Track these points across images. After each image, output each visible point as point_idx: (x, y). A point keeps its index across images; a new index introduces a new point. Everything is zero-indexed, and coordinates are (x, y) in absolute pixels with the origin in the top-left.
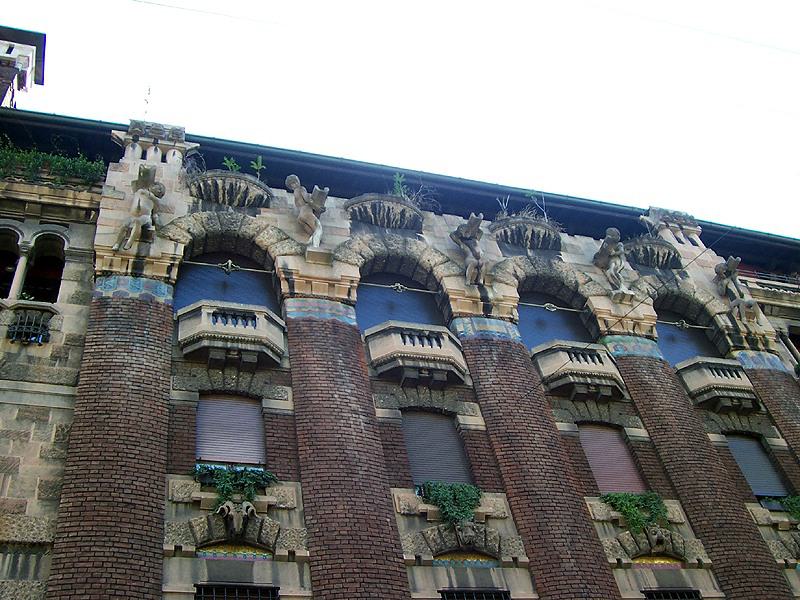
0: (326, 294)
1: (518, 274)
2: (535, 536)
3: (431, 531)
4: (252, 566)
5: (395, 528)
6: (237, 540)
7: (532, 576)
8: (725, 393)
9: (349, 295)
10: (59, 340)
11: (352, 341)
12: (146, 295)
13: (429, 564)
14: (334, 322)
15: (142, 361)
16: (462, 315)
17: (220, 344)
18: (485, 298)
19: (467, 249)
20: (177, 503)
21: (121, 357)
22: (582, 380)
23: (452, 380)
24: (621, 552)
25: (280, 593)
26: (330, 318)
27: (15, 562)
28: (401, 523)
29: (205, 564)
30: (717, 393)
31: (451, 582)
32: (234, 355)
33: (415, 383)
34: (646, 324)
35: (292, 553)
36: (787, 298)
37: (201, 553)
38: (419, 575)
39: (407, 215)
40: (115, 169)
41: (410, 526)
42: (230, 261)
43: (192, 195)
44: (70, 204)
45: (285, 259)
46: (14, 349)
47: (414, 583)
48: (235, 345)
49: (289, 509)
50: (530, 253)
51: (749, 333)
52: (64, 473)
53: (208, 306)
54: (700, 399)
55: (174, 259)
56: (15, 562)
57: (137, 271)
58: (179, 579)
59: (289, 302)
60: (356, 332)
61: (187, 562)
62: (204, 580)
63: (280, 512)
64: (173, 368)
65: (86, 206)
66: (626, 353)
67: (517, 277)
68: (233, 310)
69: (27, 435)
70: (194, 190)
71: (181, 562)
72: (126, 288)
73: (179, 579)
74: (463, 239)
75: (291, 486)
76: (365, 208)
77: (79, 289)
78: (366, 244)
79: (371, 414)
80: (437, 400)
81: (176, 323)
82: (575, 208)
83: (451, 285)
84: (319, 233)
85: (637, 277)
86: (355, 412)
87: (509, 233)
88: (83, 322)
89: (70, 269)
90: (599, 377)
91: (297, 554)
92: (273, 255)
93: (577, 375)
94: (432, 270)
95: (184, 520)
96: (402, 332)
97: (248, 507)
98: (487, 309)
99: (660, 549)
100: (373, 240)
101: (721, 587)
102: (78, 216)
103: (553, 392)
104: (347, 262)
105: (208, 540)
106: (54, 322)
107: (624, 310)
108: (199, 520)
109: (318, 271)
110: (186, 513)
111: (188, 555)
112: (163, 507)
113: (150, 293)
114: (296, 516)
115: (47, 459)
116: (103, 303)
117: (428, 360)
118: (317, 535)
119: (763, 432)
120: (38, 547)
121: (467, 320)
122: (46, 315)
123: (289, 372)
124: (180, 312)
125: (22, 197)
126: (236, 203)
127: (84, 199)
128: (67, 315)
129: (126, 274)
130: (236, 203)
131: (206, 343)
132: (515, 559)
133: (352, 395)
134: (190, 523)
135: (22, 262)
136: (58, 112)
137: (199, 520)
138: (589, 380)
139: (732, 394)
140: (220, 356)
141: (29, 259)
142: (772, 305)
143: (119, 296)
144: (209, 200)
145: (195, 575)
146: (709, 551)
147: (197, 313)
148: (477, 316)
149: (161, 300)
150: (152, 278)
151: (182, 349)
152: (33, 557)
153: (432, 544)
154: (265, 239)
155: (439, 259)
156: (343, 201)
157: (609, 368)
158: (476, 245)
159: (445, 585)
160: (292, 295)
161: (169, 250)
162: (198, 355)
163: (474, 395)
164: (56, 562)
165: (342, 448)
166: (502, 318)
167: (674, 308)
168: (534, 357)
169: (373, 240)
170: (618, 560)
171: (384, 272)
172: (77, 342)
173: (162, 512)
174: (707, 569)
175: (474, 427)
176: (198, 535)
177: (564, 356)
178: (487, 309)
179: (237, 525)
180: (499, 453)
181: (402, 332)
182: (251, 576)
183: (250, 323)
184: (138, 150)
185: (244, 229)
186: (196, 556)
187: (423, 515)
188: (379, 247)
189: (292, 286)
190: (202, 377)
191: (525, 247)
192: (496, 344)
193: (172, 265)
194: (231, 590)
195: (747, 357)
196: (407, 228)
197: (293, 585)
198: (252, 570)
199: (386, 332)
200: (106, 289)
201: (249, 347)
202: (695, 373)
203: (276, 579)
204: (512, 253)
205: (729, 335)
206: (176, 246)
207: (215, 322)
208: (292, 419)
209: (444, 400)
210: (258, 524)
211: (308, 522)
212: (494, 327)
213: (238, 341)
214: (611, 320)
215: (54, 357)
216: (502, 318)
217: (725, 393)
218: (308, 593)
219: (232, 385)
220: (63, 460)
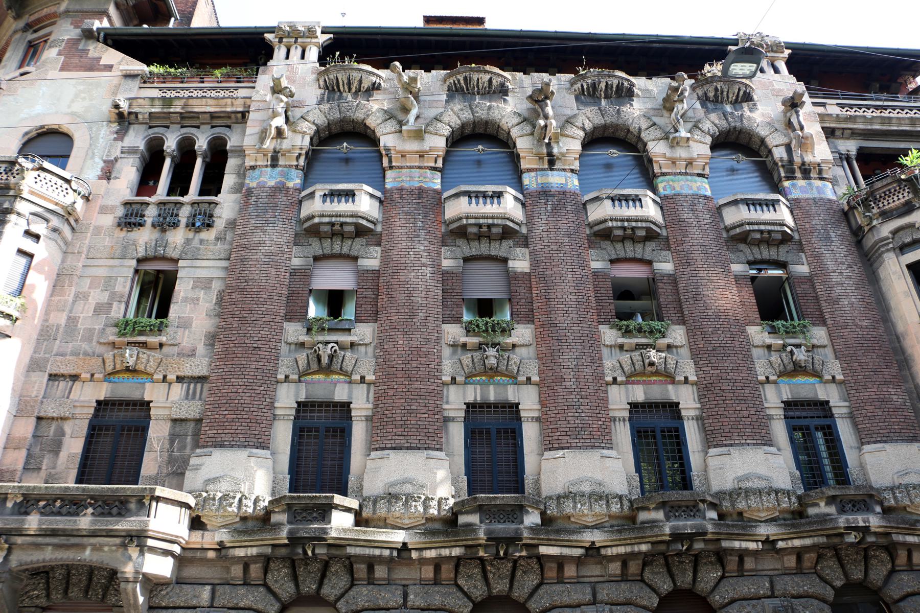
0: (417, 164)
1: (586, 126)
2: (548, 359)
3: (775, 357)
5: (440, 357)
6: (327, 370)
7: (540, 391)
8: (756, 227)
9: (436, 162)
10: (220, 224)
11: (437, 201)
12: (280, 182)
13: (775, 382)
14: (420, 189)
15: (274, 237)
16: (529, 170)
17: (326, 220)
18: (550, 154)
19: (540, 110)
20: (290, 344)
21: (258, 237)
22: (619, 224)
23: (507, 233)
24: (619, 371)
25: (520, 407)
26: (417, 185)
27: (188, 389)
28: (447, 351)
30: (610, 224)
31: (475, 397)
32: (337, 227)
33: (758, 243)
34: (701, 162)
35: (363, 378)
36: (862, 120)
37: (302, 379)
38: (614, 391)
39: (494, 82)
40: (264, 72)
41: (454, 353)
42: (345, 144)
43: (320, 88)
44: (229, 110)
45: (387, 140)
46: (191, 235)
47: (447, 397)
48: (338, 219)
49: (366, 345)
50: (603, 102)
51: (803, 164)
52: (218, 327)
53: (321, 189)
54: (732, 233)
55: (301, 149)
56: (188, 389)
57: (274, 163)
59: (389, 173)
60: (438, 193)
61: (292, 386)
62: (302, 398)
64: (297, 240)
65: (240, 109)
66: (673, 192)
67: (583, 129)
68: (338, 190)
69: (198, 300)
70: (322, 83)
72: (269, 178)
74: (537, 101)
76: (459, 81)
77: (237, 180)
78: (456, 115)
79: (437, 265)
80: (496, 249)
81: (300, 202)
82: (661, 45)
83: (523, 145)
84: (414, 112)
85: (703, 115)
86: (424, 265)
87: (585, 87)
88: (237, 208)
89: (232, 163)
90: (637, 221)
92: (378, 134)
93: (616, 220)
94: (509, 133)
96: (468, 194)
98: (552, 163)
99: (653, 369)
100: (462, 110)
101: (699, 399)
102: (237, 118)
103: (597, 234)
104: (436, 134)
106: (217, 212)
107: (681, 153)
109: (413, 146)
110: (296, 350)
111: (294, 382)
113: (283, 180)
114: (370, 349)
115: (210, 316)
116: (249, 192)
117: (487, 218)
118: (383, 365)
119: (789, 259)
120: (202, 379)
121: (533, 174)
122: (212, 206)
123: (667, 238)
124: (303, 194)
125: (196, 110)
126: (354, 90)
128: (226, 203)
129: (267, 166)
130: (354, 90)
131: (317, 220)
132: (833, 377)
133: (424, 251)
135: (168, 163)
136: (807, 42)
137: (302, 357)
138: (626, 224)
139: (762, 227)
140: (326, 228)
141: (173, 158)
142: (844, 129)
143: (261, 186)
144: (334, 90)
145: (297, 395)
146: (698, 368)
147: (312, 195)
148: (543, 170)
149: (290, 184)
150: (286, 166)
151: (448, 225)
152: (192, 385)
153: (466, 368)
154: (372, 122)
155: (516, 120)
156: (438, 74)
157: (784, 214)
158: (547, 105)
159: (470, 399)
160: (391, 168)
161: (299, 141)
162: (312, 231)
163: (525, 242)
164: (211, 389)
165: (409, 295)
166: (564, 170)
167: (734, 142)
168: (721, 206)
169: (462, 110)
170: (767, 378)
171: (477, 137)
172: (232, 225)
174: (692, 384)
175: (519, 270)
177: (608, 203)
178: (552, 163)
179: (325, 360)
180: (535, 292)
181: (468, 194)
182: (334, 394)
183: (350, 199)
184: (283, 50)
185: (357, 114)
186: (300, 381)
187: (464, 346)
188: (467, 116)
189: (390, 161)
190: (316, 247)
191: (599, 98)
192: (553, 196)
193: (300, 154)
194: (321, 404)
195: (798, 188)
196: (494, 92)
199: (457, 195)
200: (251, 182)
201: (348, 220)
202: (733, 208)
203: (350, 396)
204: (586, 104)
205: (783, 166)
206: (303, 138)
207: (324, 201)
208: (376, 274)
209: (496, 249)
212: (556, 179)
213: (340, 216)
214: (662, 162)
215: (217, 239)
216: (564, 170)
217: (756, 227)
218: (371, 406)
219: (630, 254)
220: (218, 315)
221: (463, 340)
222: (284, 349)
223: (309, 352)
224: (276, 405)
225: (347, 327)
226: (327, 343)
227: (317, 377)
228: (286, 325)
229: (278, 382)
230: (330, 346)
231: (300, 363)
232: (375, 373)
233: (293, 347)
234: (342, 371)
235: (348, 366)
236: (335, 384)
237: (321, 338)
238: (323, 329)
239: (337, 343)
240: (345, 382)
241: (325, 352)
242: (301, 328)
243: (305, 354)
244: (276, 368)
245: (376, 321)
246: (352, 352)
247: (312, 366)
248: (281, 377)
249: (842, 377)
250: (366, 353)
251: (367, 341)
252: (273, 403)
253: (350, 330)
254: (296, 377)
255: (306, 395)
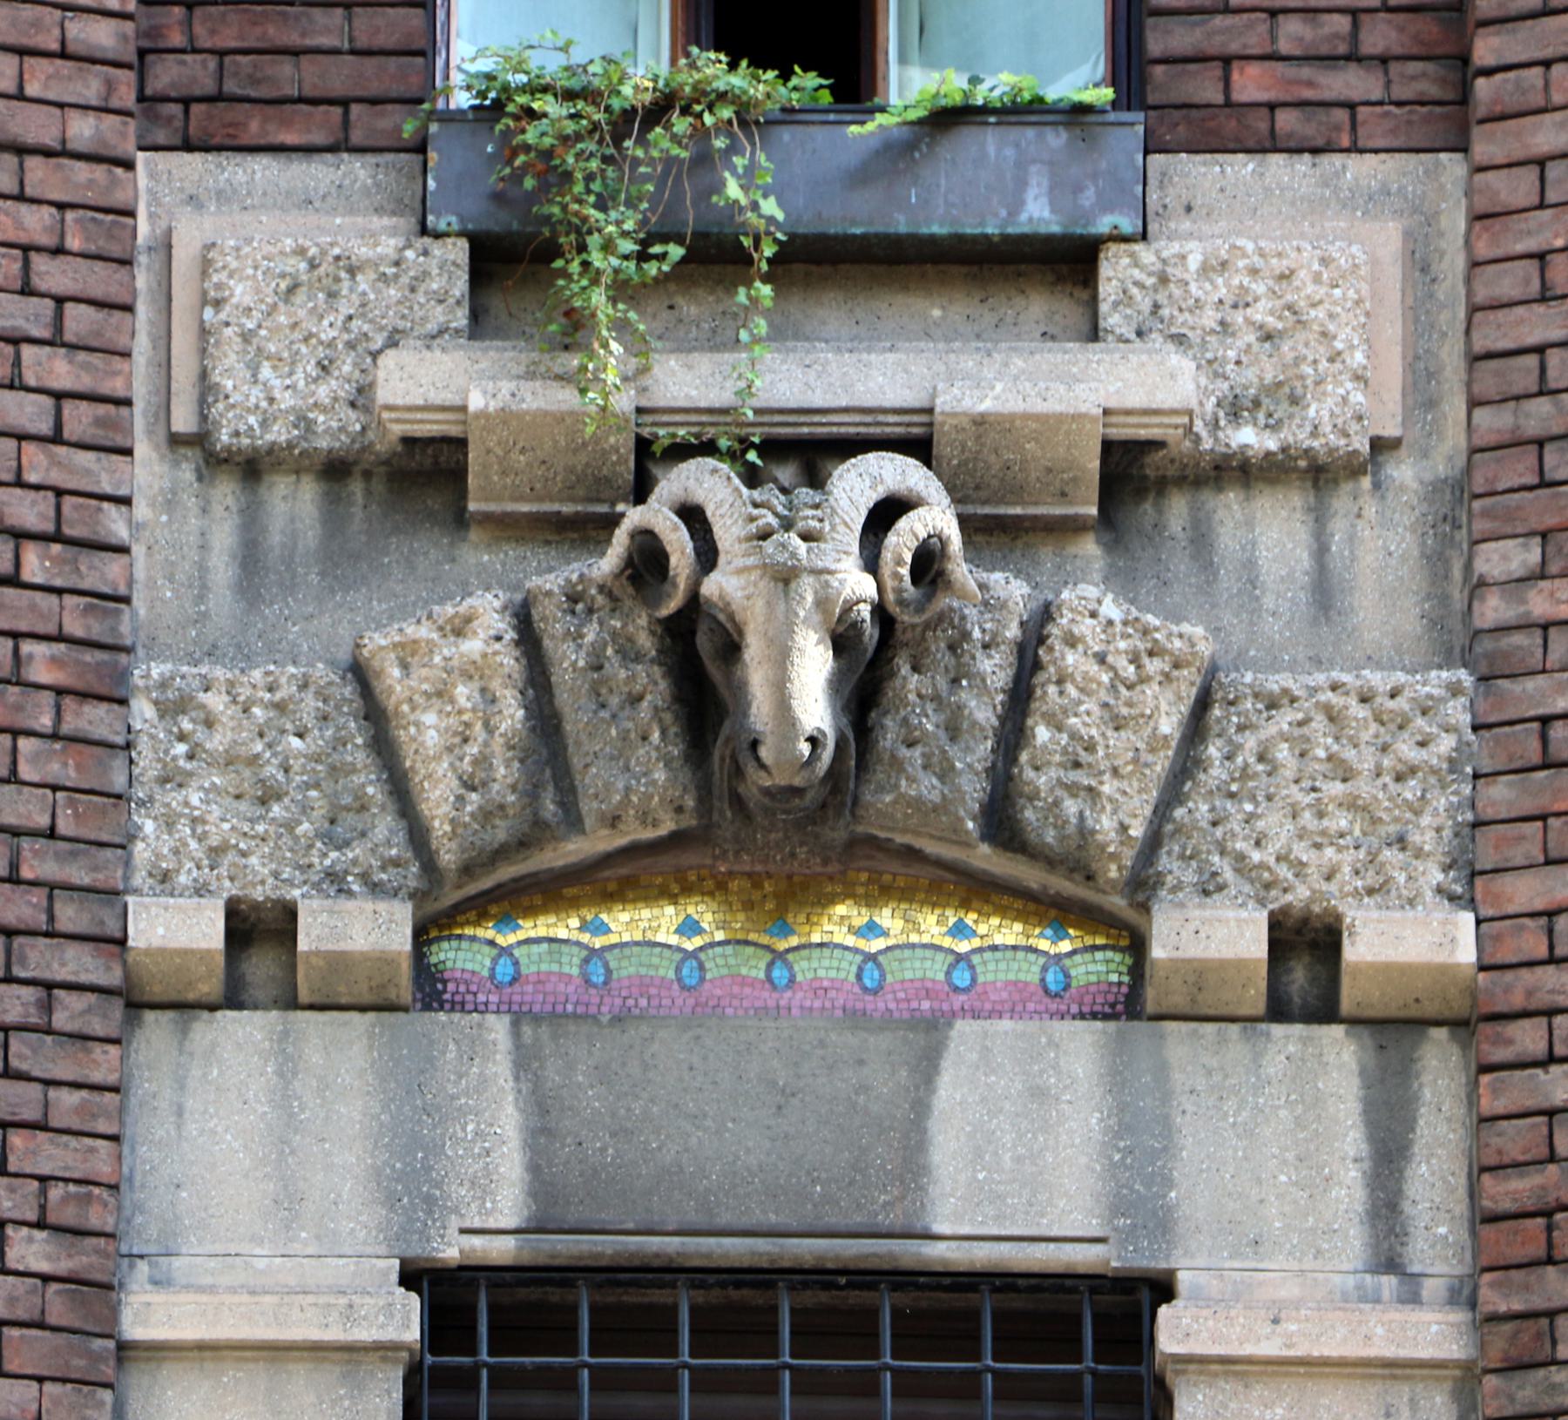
4: (927, 1066)
6: (773, 835)
20: (251, 468)
25: (1176, 1331)
29: (501, 1068)
35: (1306, 948)
37: (464, 956)
49: (1318, 475)
58: (278, 1204)
61: (341, 1050)
62: (487, 1219)
63: (1228, 507)
71: (288, 1066)
73: (278, 1204)
75: (1372, 202)
91: (1354, 952)
95: (318, 629)
97: (887, 512)
105: (522, 844)
108: (452, 649)
110: (341, 561)
112: (115, 525)
114: (1381, 540)
119: (1173, 1265)
127: (1507, 1191)
134: (360, 674)
137: (452, 649)
145: (411, 1181)
173: (104, 573)
176: (439, 799)
186: (430, 989)
194: (738, 1304)
197: (1289, 1241)
198: (920, 1108)
210: (995, 669)
211: (1493, 609)
218: (1435, 1333)
221: (445, 378)
222: (169, 532)
223: (551, 576)
224: (148, 1315)
225: (1038, 213)
226: (802, 452)
227: (649, 926)
228: (163, 185)
229: (135, 1002)
230: (858, 484)
231: (426, 733)
232: (1470, 880)
233: (294, 505)
234: (1016, 861)
235: (1099, 774)
236: (925, 1031)
237: (688, 382)
238: (716, 257)
239: (919, 447)
240: (1061, 1001)
241: (790, 606)
242: (382, 239)
243: (489, 612)
244: (102, 806)
245: (1449, 121)
246: (1122, 580)
247: (600, 781)
248: (177, 928)
249: (1455, 941)
250: (1325, 592)
251: (1331, 416)
252: (99, 1291)
253: (1069, 263)
254: (372, 929)
255: (542, 1182)
